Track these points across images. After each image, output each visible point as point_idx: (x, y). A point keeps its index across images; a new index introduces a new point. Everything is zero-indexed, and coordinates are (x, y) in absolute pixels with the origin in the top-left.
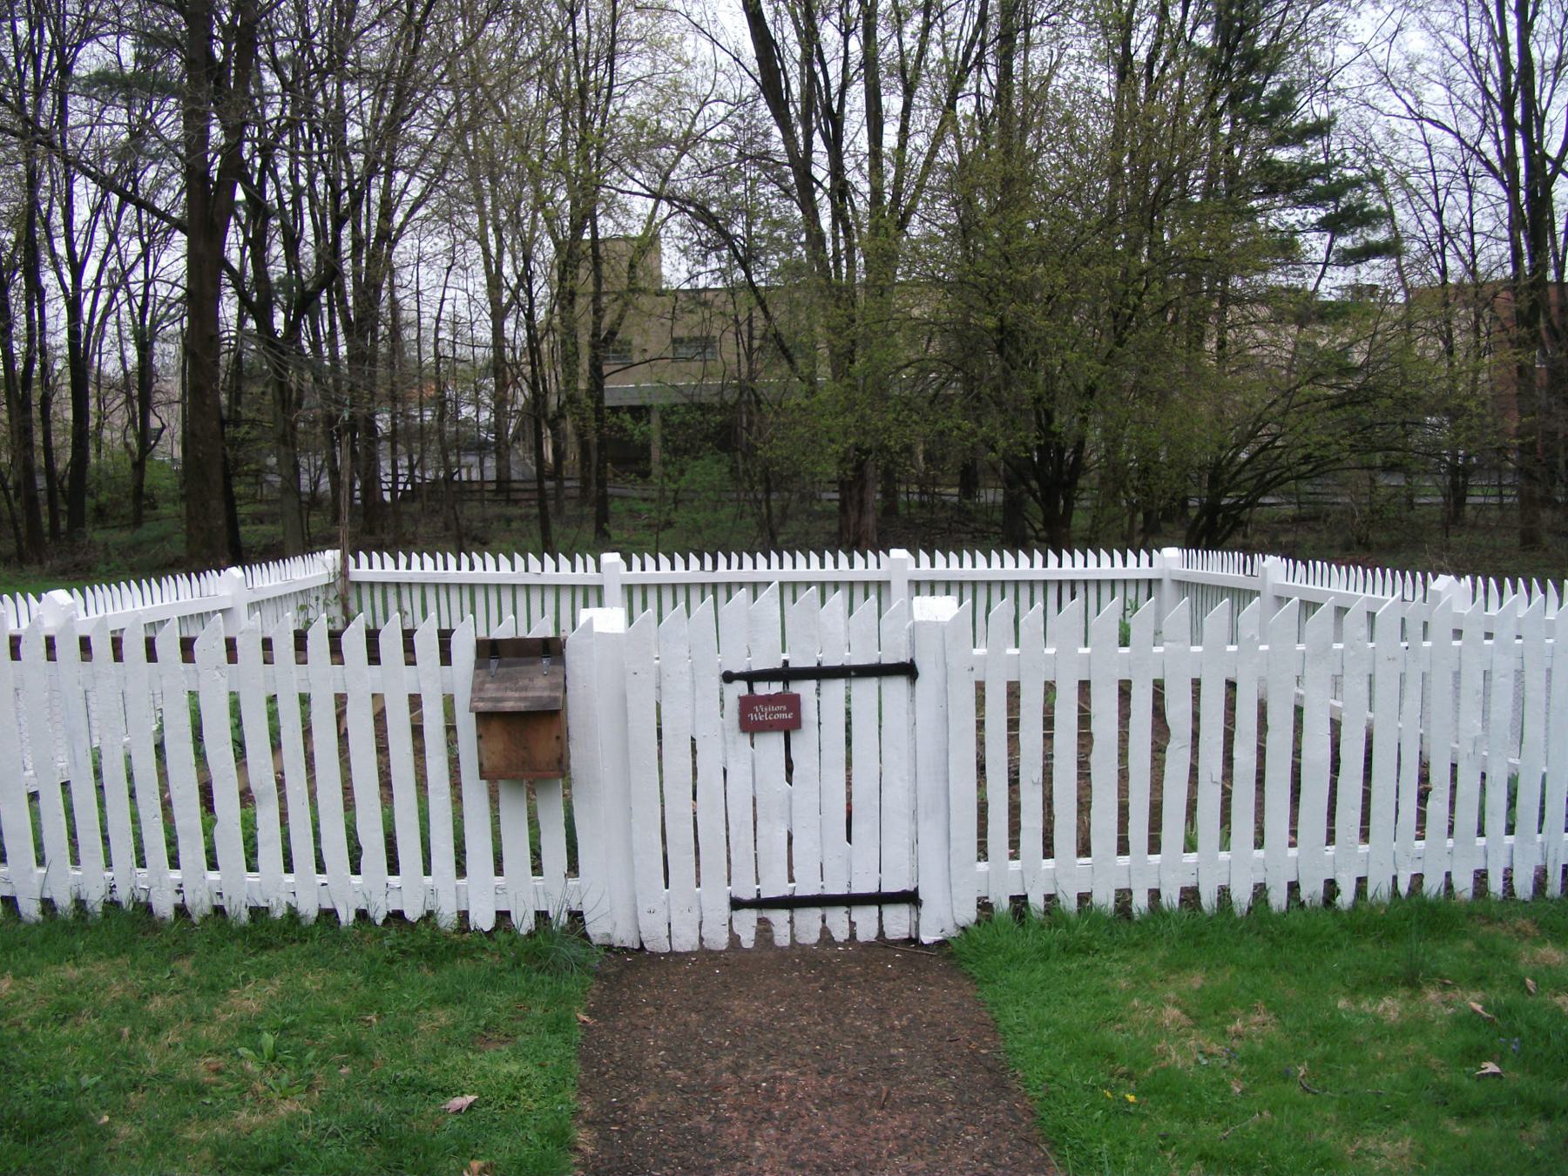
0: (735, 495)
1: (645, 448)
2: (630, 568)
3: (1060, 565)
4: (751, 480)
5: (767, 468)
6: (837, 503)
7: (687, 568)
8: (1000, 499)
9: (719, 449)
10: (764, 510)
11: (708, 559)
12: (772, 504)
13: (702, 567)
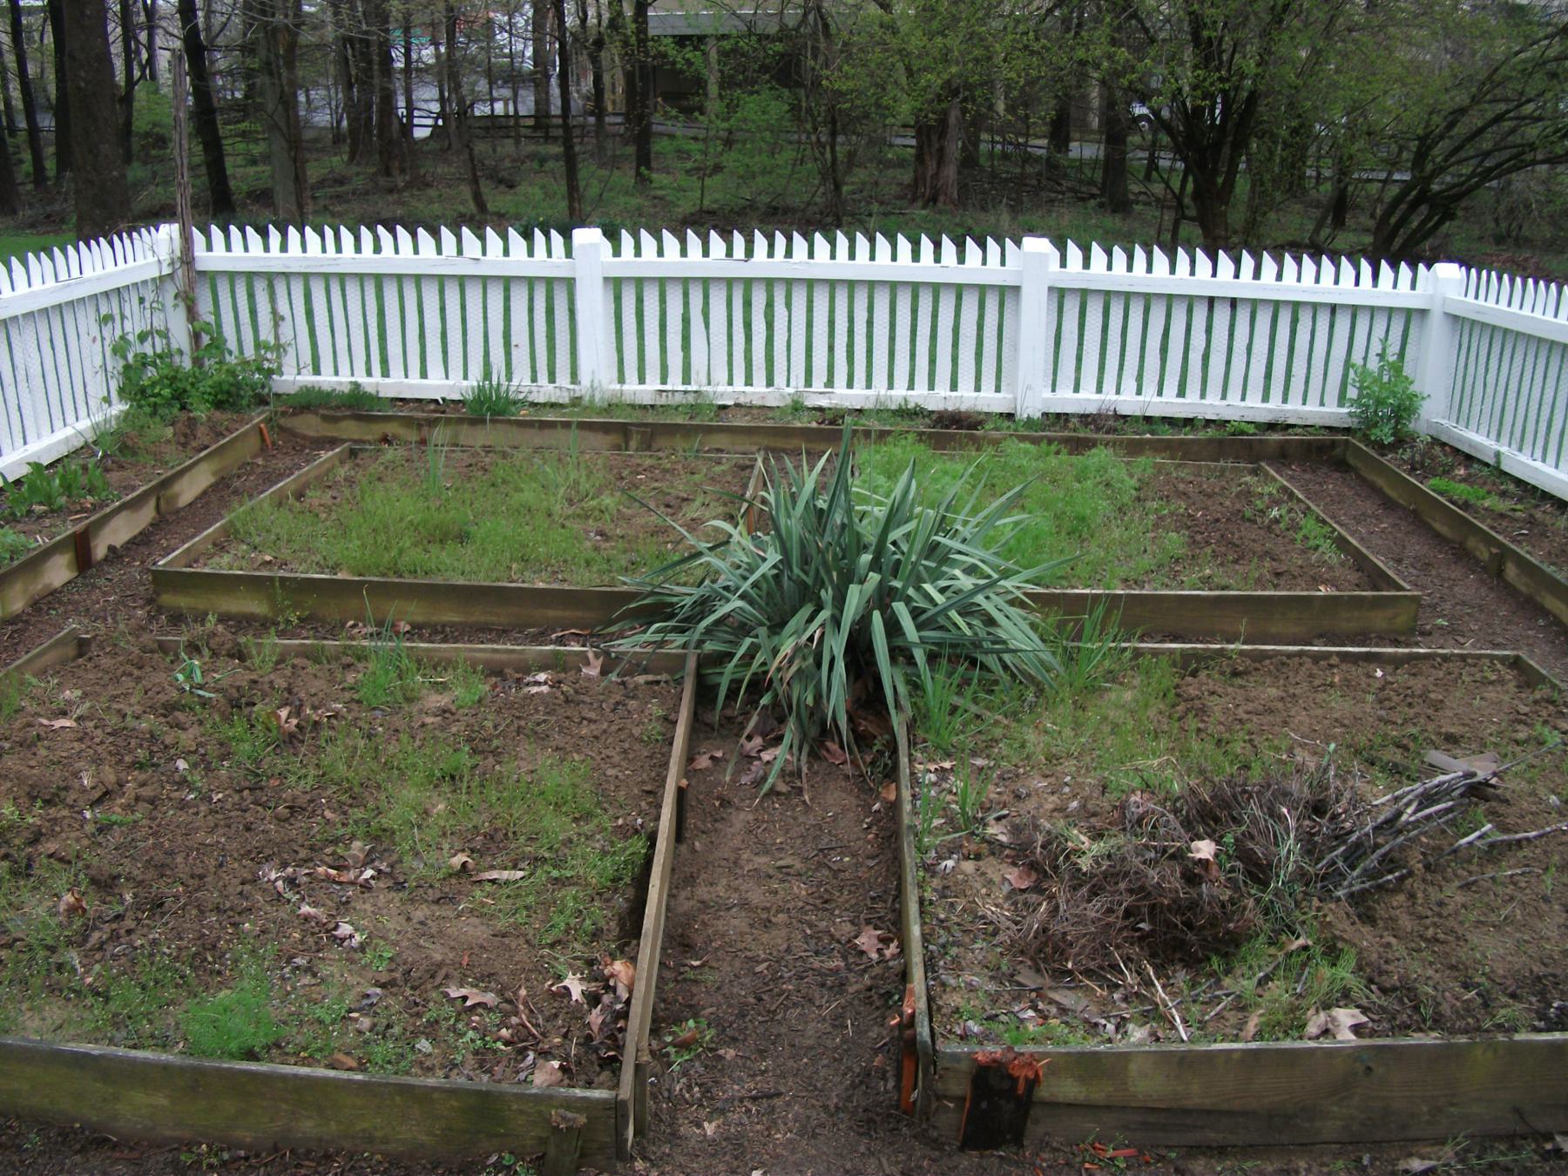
0: (796, 137)
1: (700, 83)
2: (617, 252)
3: (1279, 277)
4: (814, 120)
5: (833, 107)
6: (912, 151)
7: (706, 253)
8: (1074, 145)
9: (779, 81)
10: (828, 156)
11: (738, 239)
12: (838, 148)
13: (729, 253)
